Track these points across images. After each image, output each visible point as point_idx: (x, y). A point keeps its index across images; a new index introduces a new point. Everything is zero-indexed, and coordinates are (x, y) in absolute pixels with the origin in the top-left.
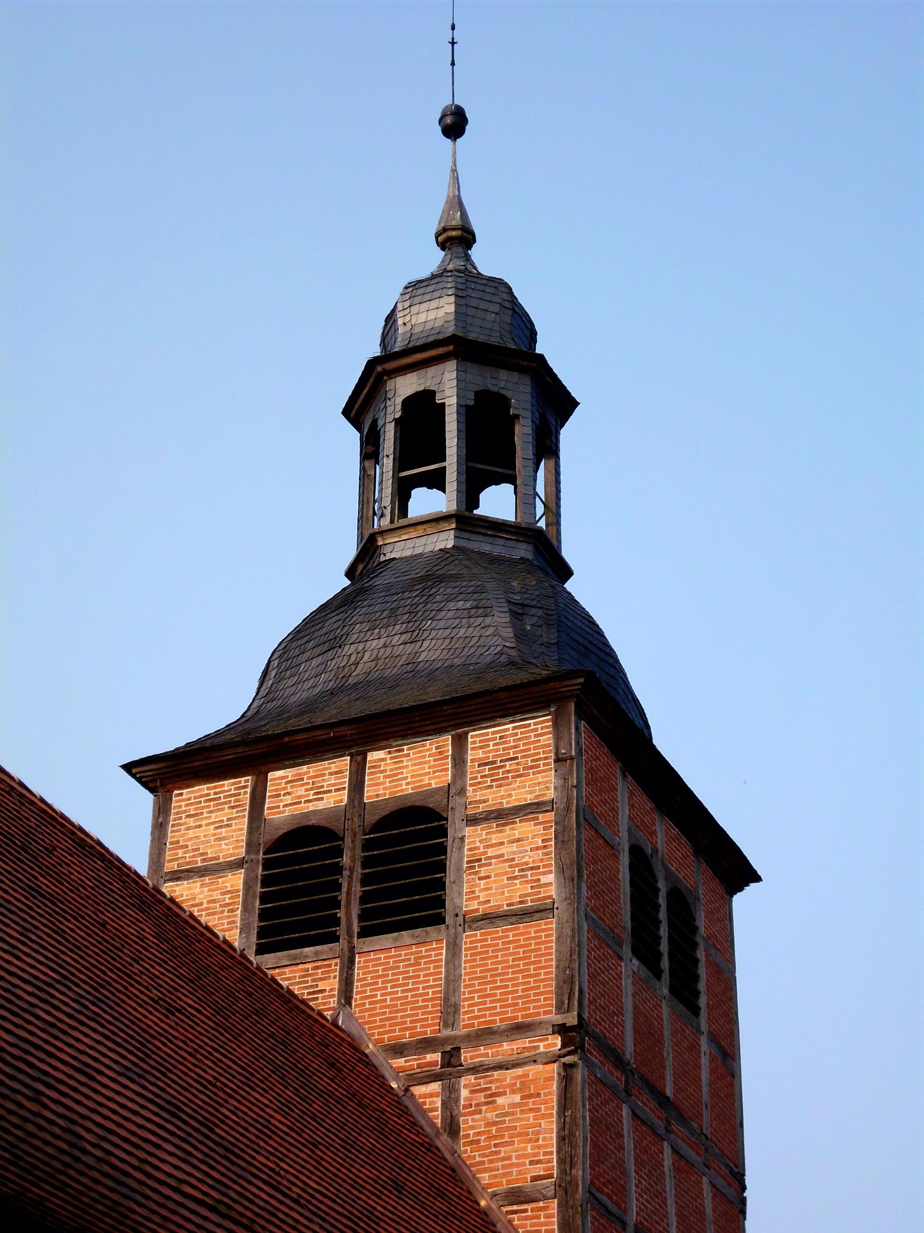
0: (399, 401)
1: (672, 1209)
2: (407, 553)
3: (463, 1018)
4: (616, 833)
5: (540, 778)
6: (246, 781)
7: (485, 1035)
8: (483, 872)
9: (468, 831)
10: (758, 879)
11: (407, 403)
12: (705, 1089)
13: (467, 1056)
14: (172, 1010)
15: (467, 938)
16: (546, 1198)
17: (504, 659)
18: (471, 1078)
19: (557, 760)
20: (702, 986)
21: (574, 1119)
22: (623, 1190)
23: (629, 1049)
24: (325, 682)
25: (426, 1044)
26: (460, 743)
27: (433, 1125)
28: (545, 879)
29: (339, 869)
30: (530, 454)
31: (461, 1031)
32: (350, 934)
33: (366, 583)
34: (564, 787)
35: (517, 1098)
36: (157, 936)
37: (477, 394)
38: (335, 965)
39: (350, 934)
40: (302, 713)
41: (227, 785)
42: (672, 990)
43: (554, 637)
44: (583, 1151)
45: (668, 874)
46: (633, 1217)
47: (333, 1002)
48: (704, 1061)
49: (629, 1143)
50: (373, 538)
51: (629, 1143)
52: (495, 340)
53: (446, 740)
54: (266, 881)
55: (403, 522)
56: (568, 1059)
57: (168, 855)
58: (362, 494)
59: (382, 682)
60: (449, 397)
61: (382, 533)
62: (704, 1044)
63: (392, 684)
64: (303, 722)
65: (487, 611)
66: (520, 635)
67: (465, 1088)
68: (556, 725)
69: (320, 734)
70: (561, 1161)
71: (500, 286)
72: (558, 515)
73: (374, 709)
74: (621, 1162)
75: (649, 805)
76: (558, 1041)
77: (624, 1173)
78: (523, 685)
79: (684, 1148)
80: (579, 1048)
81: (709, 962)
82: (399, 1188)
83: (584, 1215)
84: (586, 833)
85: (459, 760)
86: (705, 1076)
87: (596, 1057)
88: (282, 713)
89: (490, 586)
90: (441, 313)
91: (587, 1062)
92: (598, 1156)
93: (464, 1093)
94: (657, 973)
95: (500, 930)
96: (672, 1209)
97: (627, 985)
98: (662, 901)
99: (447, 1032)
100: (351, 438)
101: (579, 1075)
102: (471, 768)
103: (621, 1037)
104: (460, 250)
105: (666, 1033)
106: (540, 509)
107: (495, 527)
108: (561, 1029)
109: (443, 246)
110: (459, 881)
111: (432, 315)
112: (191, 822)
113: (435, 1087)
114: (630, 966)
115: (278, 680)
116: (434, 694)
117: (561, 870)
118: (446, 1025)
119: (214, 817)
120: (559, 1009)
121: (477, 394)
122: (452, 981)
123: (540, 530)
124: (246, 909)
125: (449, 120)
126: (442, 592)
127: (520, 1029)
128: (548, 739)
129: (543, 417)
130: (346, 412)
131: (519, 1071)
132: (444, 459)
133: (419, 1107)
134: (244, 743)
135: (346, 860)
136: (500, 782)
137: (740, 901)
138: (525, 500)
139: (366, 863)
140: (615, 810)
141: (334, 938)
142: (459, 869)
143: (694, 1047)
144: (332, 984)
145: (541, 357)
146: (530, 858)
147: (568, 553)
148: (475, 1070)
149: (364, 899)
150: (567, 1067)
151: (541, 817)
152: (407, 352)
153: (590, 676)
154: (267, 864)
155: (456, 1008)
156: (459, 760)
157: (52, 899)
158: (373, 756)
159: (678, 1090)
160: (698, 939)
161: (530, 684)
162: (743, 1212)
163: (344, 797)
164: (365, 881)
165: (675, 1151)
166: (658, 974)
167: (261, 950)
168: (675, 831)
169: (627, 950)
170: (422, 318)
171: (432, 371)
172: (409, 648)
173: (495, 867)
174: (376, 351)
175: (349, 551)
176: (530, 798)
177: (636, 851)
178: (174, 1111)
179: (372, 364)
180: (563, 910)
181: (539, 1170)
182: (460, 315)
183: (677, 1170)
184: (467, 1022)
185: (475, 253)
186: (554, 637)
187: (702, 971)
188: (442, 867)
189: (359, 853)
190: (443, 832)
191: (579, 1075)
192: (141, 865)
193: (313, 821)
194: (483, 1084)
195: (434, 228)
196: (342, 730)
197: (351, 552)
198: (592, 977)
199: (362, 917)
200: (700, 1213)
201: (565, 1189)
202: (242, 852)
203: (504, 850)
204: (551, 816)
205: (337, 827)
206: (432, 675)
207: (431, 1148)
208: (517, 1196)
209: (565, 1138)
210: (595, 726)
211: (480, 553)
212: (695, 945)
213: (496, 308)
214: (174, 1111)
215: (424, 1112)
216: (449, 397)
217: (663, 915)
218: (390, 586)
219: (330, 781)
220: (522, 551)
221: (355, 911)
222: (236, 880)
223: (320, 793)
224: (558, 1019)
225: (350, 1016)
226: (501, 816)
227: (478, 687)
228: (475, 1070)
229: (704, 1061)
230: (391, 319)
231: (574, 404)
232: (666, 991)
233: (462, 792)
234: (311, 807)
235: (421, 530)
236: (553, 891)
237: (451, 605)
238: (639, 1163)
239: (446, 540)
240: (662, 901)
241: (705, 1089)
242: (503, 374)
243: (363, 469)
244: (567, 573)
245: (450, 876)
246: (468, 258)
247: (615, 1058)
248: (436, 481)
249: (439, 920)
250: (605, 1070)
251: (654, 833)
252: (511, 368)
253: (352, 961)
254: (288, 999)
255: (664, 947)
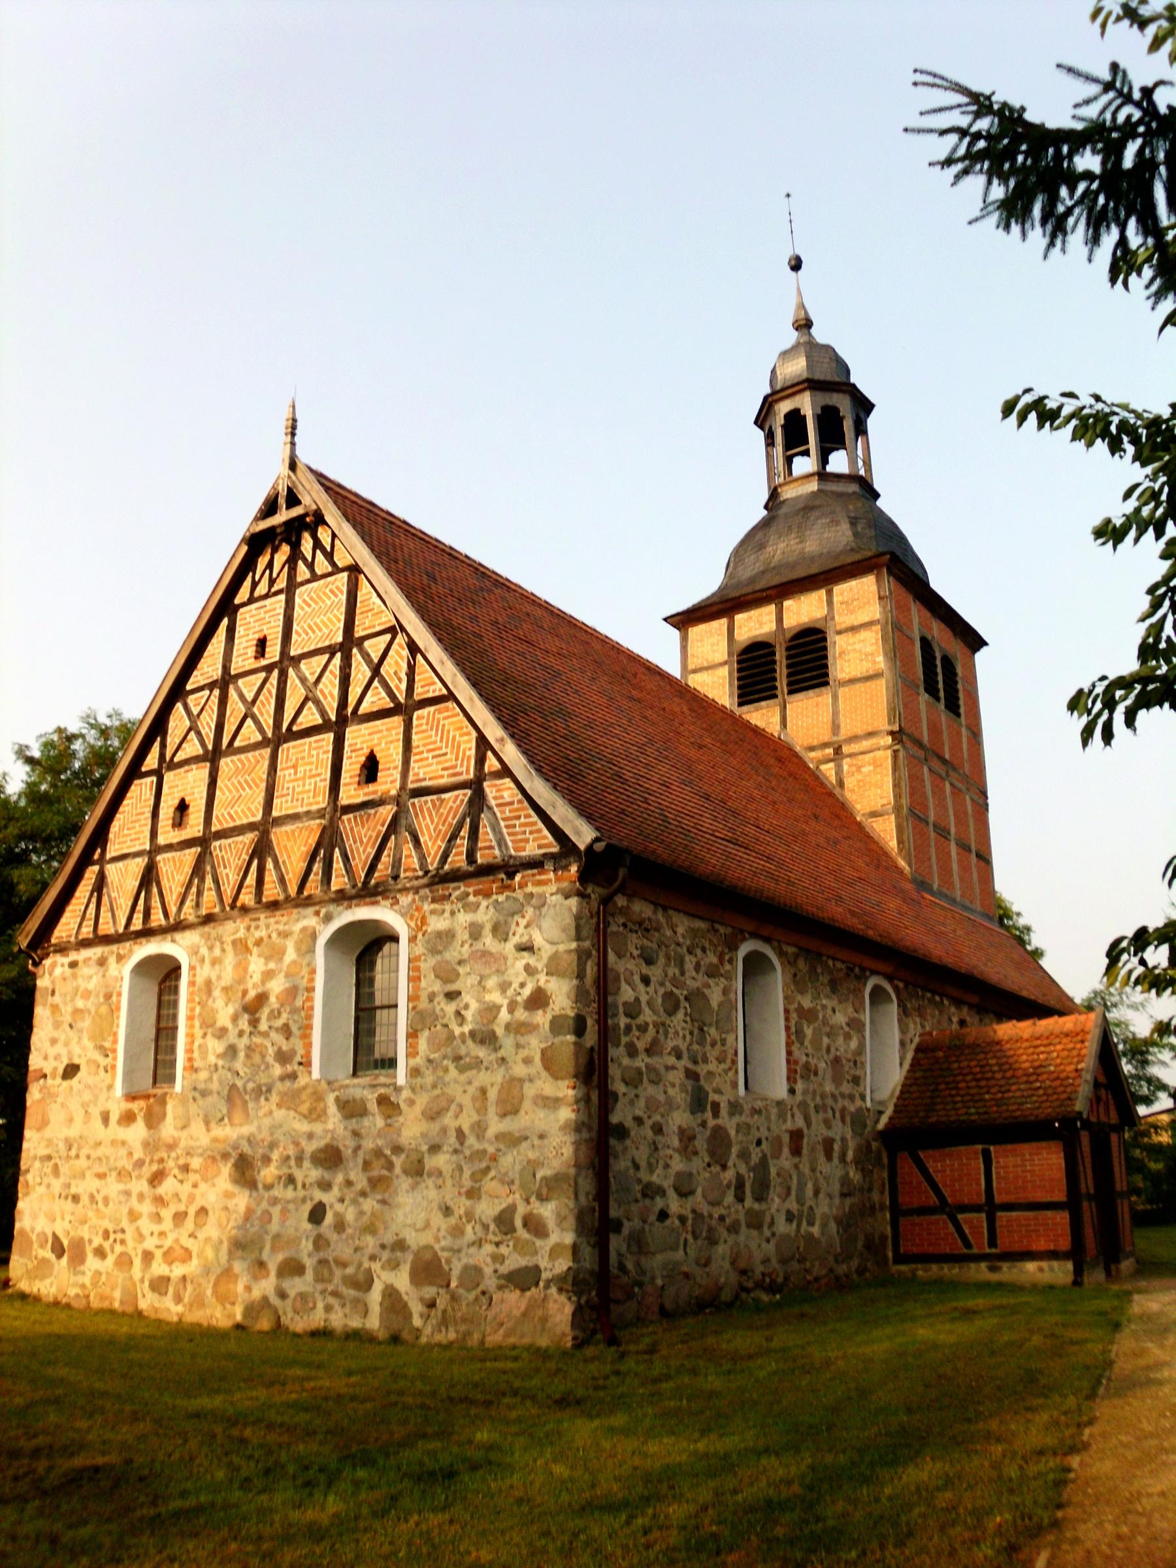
1: (951, 812)
4: (913, 631)
6: (724, 621)
7: (854, 738)
9: (837, 638)
10: (986, 644)
11: (787, 416)
13: (846, 749)
14: (701, 747)
15: (842, 692)
16: (888, 814)
18: (848, 760)
19: (880, 598)
20: (961, 702)
21: (900, 777)
22: (926, 807)
23: (926, 739)
24: (759, 567)
25: (825, 745)
26: (830, 593)
27: (831, 783)
30: (853, 435)
35: (872, 768)
36: (690, 709)
38: (777, 710)
42: (947, 707)
43: (873, 533)
44: (905, 789)
47: (778, 728)
48: (964, 739)
49: (928, 784)
50: (775, 489)
51: (928, 784)
53: (823, 592)
54: (739, 671)
56: (896, 747)
57: (689, 661)
60: (808, 412)
61: (781, 485)
62: (964, 731)
63: (792, 566)
64: (749, 589)
65: (837, 523)
66: (856, 535)
67: (846, 763)
68: (878, 580)
69: (759, 595)
70: (895, 796)
71: (828, 348)
73: (785, 580)
74: (924, 793)
76: (890, 738)
77: (926, 798)
78: (858, 562)
79: (957, 783)
80: (900, 742)
81: (964, 690)
82: (816, 817)
84: (897, 634)
85: (830, 602)
86: (965, 746)
87: (909, 745)
88: (738, 585)
91: (904, 747)
94: (938, 699)
96: (951, 812)
97: (923, 707)
98: (938, 662)
99: (835, 739)
100: (759, 435)
101: (901, 754)
106: (860, 463)
107: (838, 477)
108: (892, 733)
109: (797, 329)
113: (831, 765)
114: (924, 697)
115: (735, 568)
116: (814, 570)
117: (885, 654)
120: (889, 723)
122: (835, 714)
123: (861, 477)
124: (730, 685)
125: (793, 263)
127: (871, 734)
128: (874, 588)
130: (756, 423)
131: (872, 755)
132: (807, 442)
133: (824, 775)
134: (722, 602)
135: (777, 657)
136: (852, 612)
137: (980, 657)
138: (853, 461)
139: (788, 658)
140: (911, 621)
141: (775, 696)
142: (835, 658)
143: (959, 734)
144: (777, 719)
146: (869, 649)
147: (877, 486)
148: (851, 755)
149: (789, 676)
150: (895, 752)
151: (874, 628)
152: (783, 390)
154: (739, 662)
156: (830, 602)
157: (639, 701)
159: (952, 755)
162: (987, 810)
164: (788, 666)
165: (951, 784)
167: (740, 704)
168: (943, 626)
169: (922, 690)
170: (790, 370)
173: (852, 655)
174: (768, 390)
175: (765, 496)
178: (707, 797)
179: (766, 398)
180: (888, 674)
181: (885, 801)
182: (809, 366)
183: (952, 793)
184: (844, 733)
185: (813, 331)
186: (873, 533)
187: (961, 695)
188: (826, 657)
189: (784, 654)
190: (825, 639)
191: (901, 754)
192: (675, 670)
193: (760, 639)
195: (791, 320)
196: (770, 592)
198: (905, 706)
199: (789, 684)
201: (897, 809)
202: (726, 657)
203: (857, 646)
204: (879, 627)
205: (771, 641)
206: (812, 559)
207: (831, 794)
208: (874, 814)
209: (896, 785)
212: (956, 683)
214: (707, 797)
215: (827, 778)
216: (808, 412)
217: (939, 670)
219: (766, 618)
220: (854, 488)
221: (785, 682)
222: (724, 671)
223: (761, 624)
224: (889, 728)
225: (786, 735)
226: (853, 629)
227: (836, 564)
228: (851, 755)
229: (964, 739)
230: (773, 371)
231: (872, 406)
232: (943, 707)
233: (833, 618)
235: (800, 482)
236: (882, 666)
238: (934, 793)
239: (813, 486)
240: (938, 662)
243: (767, 452)
244: (876, 496)
245: (830, 661)
246: (810, 334)
247: (919, 744)
248: (806, 453)
249: (827, 684)
250: (915, 751)
251: (931, 629)
252: (838, 391)
253: (785, 707)
254: (756, 731)
255: (941, 686)
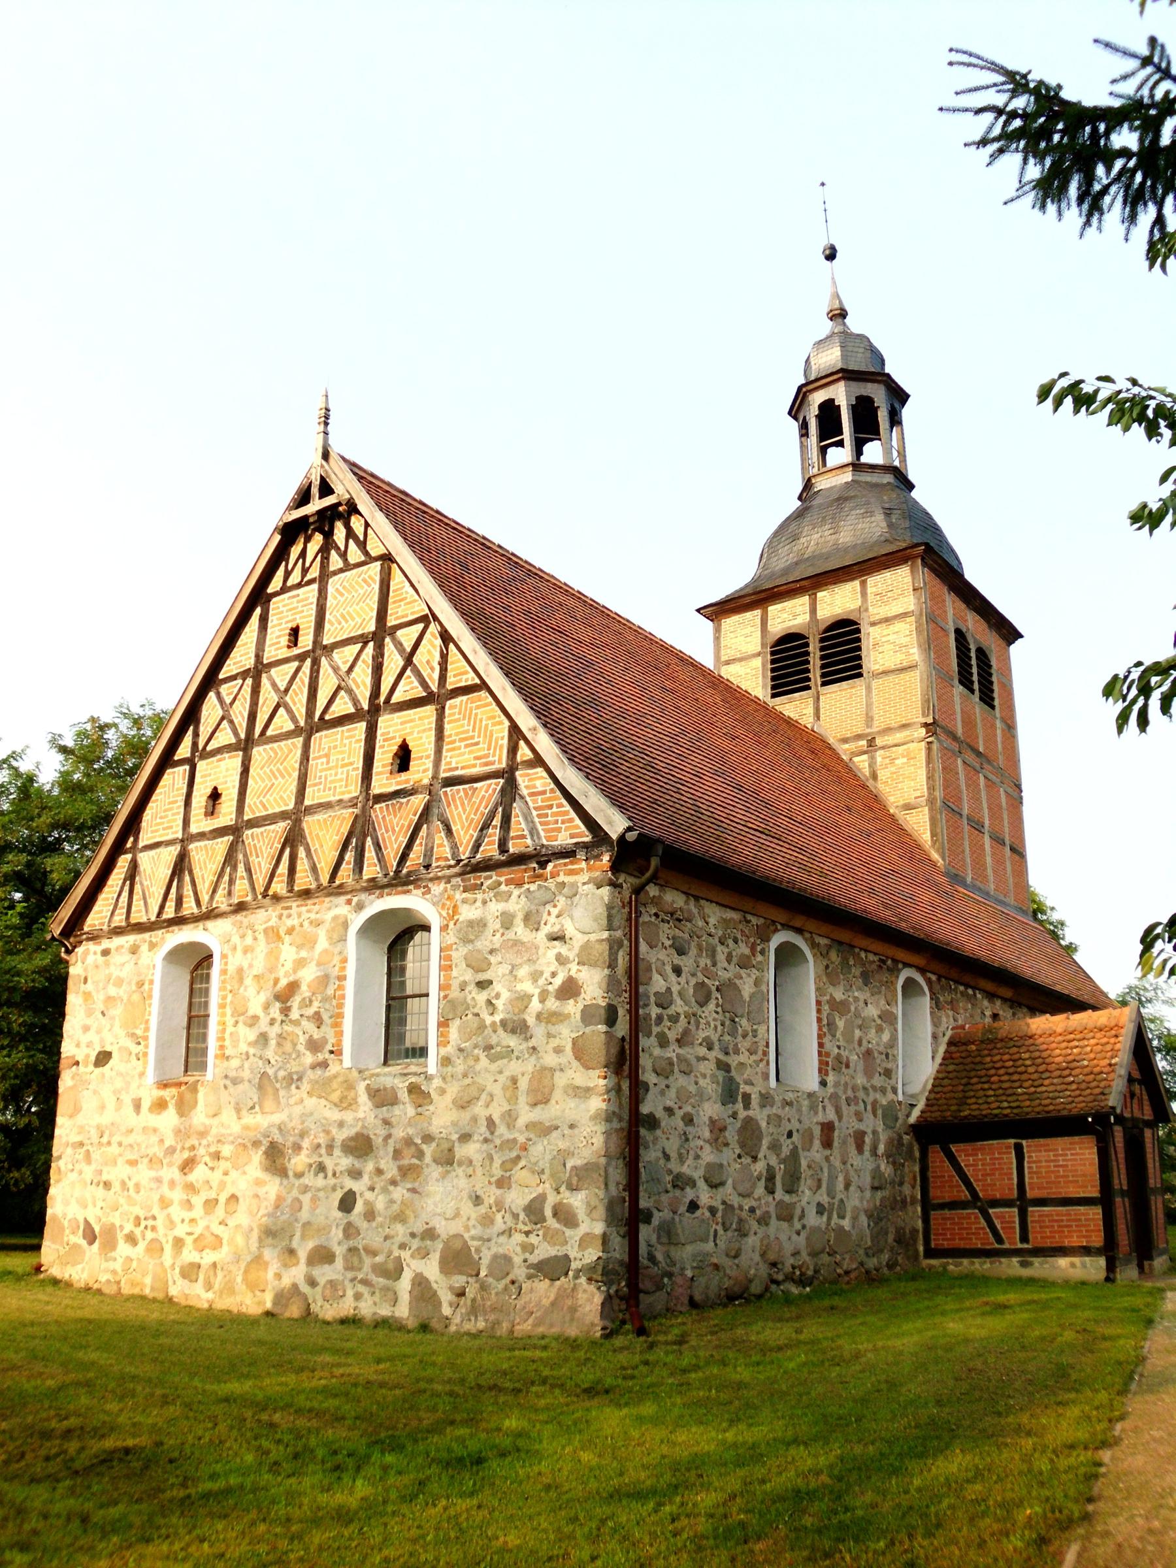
0: (816, 406)
2: (828, 486)
3: (876, 723)
5: (906, 599)
7: (888, 730)
8: (881, 649)
9: (871, 630)
10: (1021, 636)
12: (1000, 746)
13: (879, 742)
15: (875, 684)
17: (883, 539)
20: (996, 695)
21: (934, 768)
22: (960, 799)
23: (960, 732)
24: (792, 558)
25: (859, 737)
26: (863, 584)
28: (912, 651)
29: (808, 654)
31: (875, 730)
32: (816, 685)
33: (807, 504)
34: (919, 603)
35: (905, 760)
37: (857, 398)
38: (811, 701)
39: (816, 685)
40: (782, 575)
41: (748, 615)
42: (981, 699)
43: (907, 524)
44: (939, 783)
45: (975, 641)
46: (965, 812)
47: (811, 719)
48: (999, 732)
49: (962, 776)
50: (809, 479)
51: (962, 776)
52: (863, 369)
53: (856, 583)
55: (825, 469)
57: (723, 652)
58: (802, 455)
59: (821, 556)
62: (999, 724)
63: (827, 557)
65: (872, 514)
66: (890, 525)
68: (912, 572)
69: (793, 586)
70: (928, 788)
71: (862, 338)
72: (905, 456)
75: (963, 606)
77: (960, 791)
79: (990, 776)
83: (941, 814)
85: (864, 593)
86: (999, 739)
87: (943, 737)
89: (872, 500)
90: (834, 356)
91: (938, 739)
92: (947, 785)
93: (879, 759)
95: (891, 677)
96: (985, 805)
97: (957, 699)
100: (794, 426)
101: (935, 747)
102: (870, 597)
103: (955, 726)
104: (840, 320)
105: (978, 721)
106: (895, 454)
108: (926, 725)
110: (868, 655)
111: (829, 358)
112: (732, 635)
113: (865, 757)
115: (769, 559)
117: (920, 646)
118: (868, 727)
119: (743, 632)
120: (923, 715)
121: (857, 398)
122: (869, 705)
124: (764, 676)
125: (827, 252)
126: (848, 505)
127: (904, 726)
128: (909, 579)
129: (892, 406)
130: (790, 413)
131: (905, 747)
132: (842, 434)
136: (886, 603)
137: (1016, 649)
138: (887, 451)
140: (945, 612)
141: (808, 688)
142: (868, 649)
143: (993, 726)
144: (810, 710)
145: (888, 375)
146: (904, 641)
148: (883, 748)
149: (823, 667)
151: (908, 619)
152: (817, 380)
153: (927, 545)
154: (772, 653)
155: (872, 719)
156: (864, 593)
158: (819, 595)
159: (986, 748)
160: (993, 671)
161: (897, 551)
163: (807, 617)
164: (822, 658)
166: (972, 691)
169: (956, 682)
170: (824, 360)
171: (832, 388)
172: (833, 537)
173: (887, 647)
176: (901, 611)
177: (958, 632)
179: (800, 388)
180: (922, 666)
183: (987, 786)
186: (907, 524)
190: (858, 631)
191: (935, 747)
192: (708, 661)
194: (888, 754)
195: (826, 310)
197: (800, 488)
198: (939, 698)
200: (1000, 806)
201: (931, 801)
202: (759, 649)
206: (846, 550)
207: (864, 787)
208: (908, 807)
209: (930, 778)
210: (933, 570)
211: (866, 483)
213: (861, 350)
215: (859, 770)
218: (821, 504)
220: (888, 478)
222: (757, 663)
223: (795, 616)
224: (924, 720)
225: (820, 726)
227: (871, 556)
228: (883, 748)
229: (999, 732)
230: (808, 361)
231: (908, 396)
233: (867, 610)
234: (791, 623)
237: (853, 512)
238: (968, 786)
239: (847, 476)
241: (1000, 746)
242: (869, 385)
243: (801, 442)
244: (911, 486)
245: (864, 653)
246: (844, 324)
247: (955, 738)
248: (840, 444)
249: (860, 675)
250: (948, 742)
253: (818, 698)
254: (789, 723)
255: (975, 678)
